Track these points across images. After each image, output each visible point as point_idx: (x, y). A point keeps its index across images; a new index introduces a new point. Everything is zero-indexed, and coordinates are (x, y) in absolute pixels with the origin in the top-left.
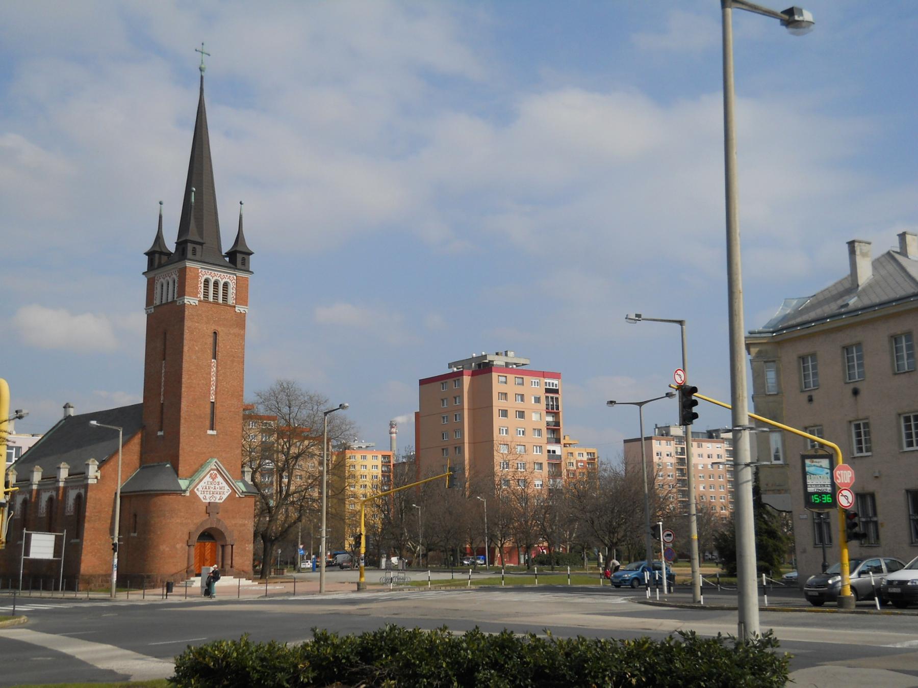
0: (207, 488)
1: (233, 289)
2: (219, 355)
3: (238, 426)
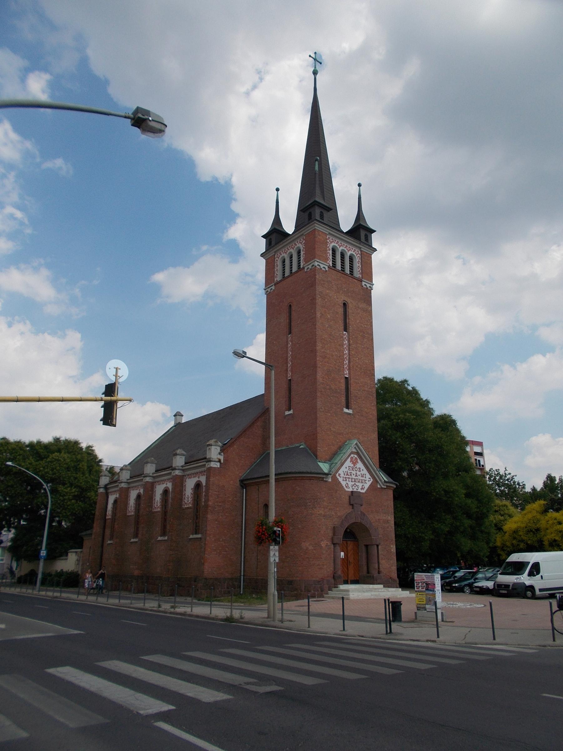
0: (349, 474)
1: (359, 264)
2: (351, 329)
3: (372, 408)
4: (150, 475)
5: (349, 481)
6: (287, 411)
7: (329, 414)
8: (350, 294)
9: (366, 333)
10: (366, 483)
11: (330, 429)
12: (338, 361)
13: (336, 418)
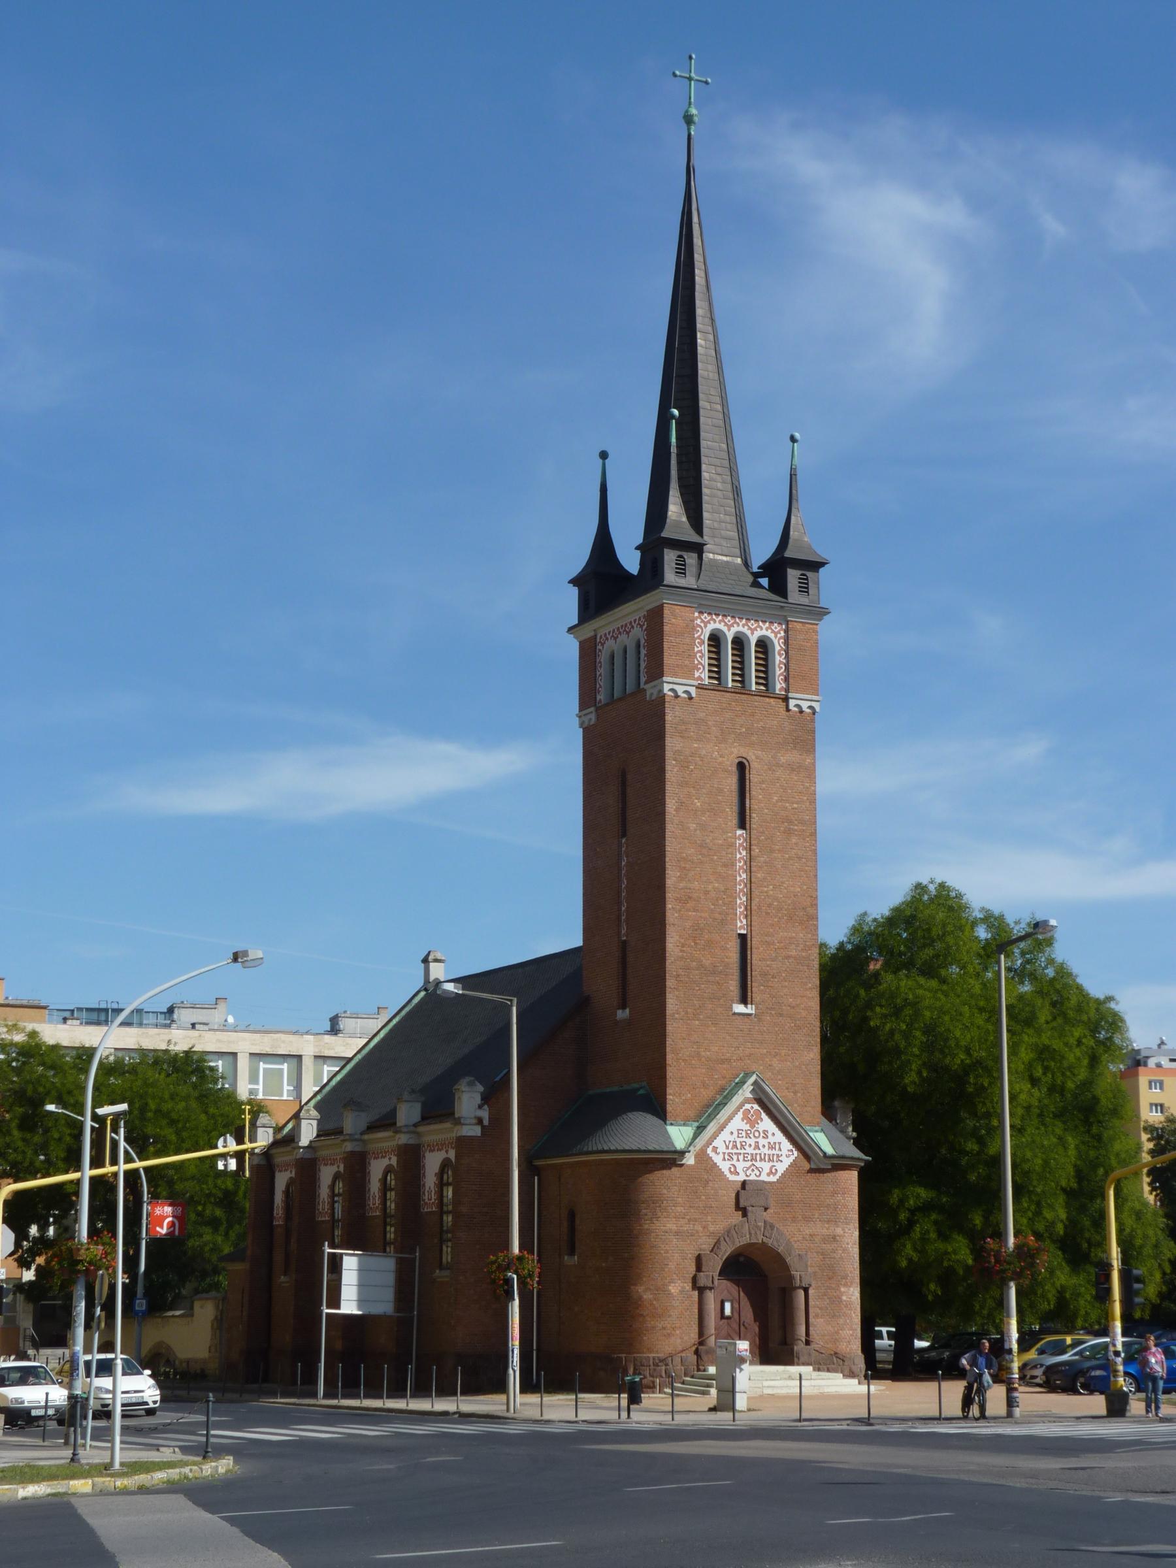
0: (739, 1146)
2: (755, 819)
4: (356, 1137)
5: (738, 1160)
6: (619, 1009)
7: (697, 1022)
8: (754, 738)
9: (796, 822)
10: (781, 1161)
11: (698, 1053)
12: (721, 902)
13: (714, 1029)
